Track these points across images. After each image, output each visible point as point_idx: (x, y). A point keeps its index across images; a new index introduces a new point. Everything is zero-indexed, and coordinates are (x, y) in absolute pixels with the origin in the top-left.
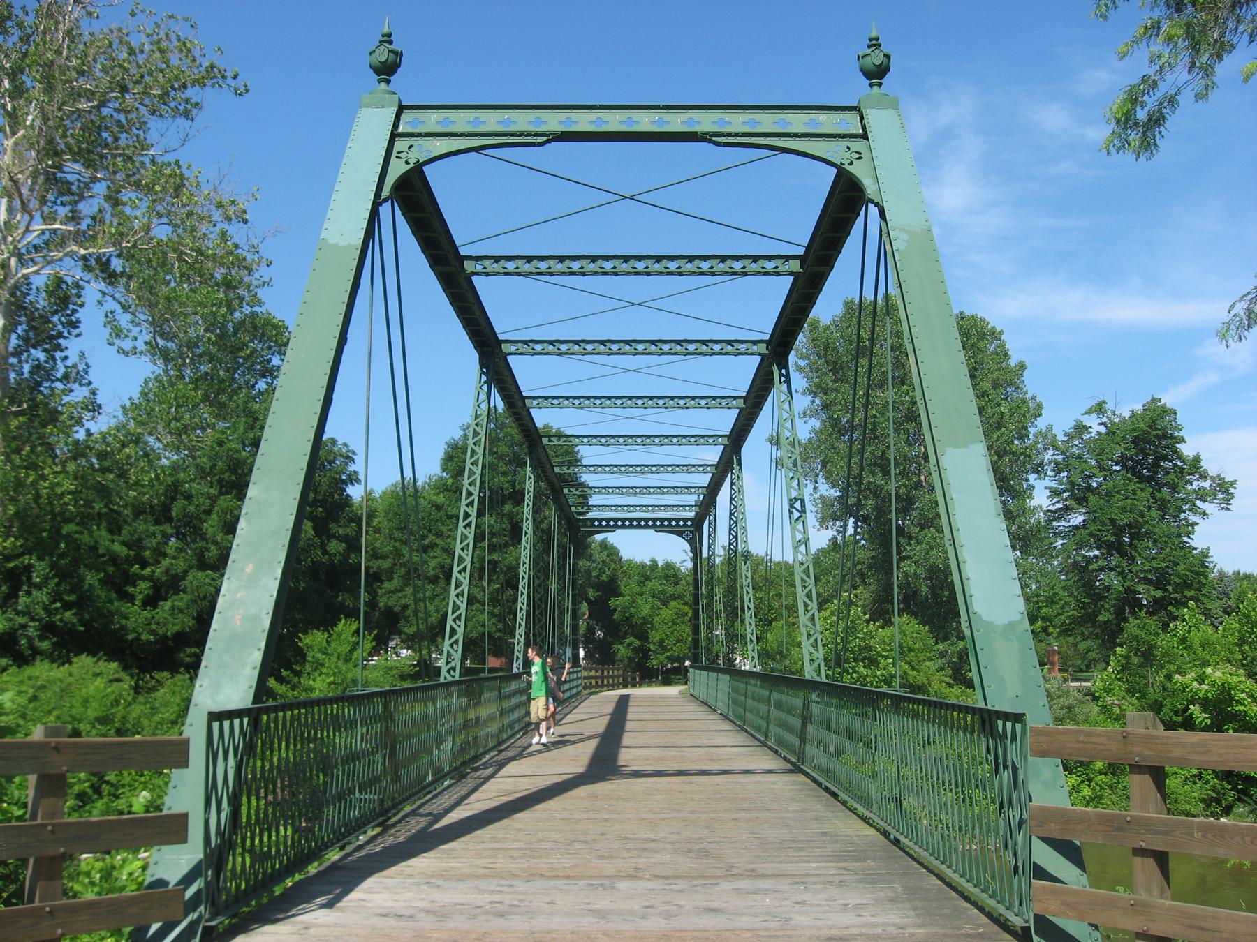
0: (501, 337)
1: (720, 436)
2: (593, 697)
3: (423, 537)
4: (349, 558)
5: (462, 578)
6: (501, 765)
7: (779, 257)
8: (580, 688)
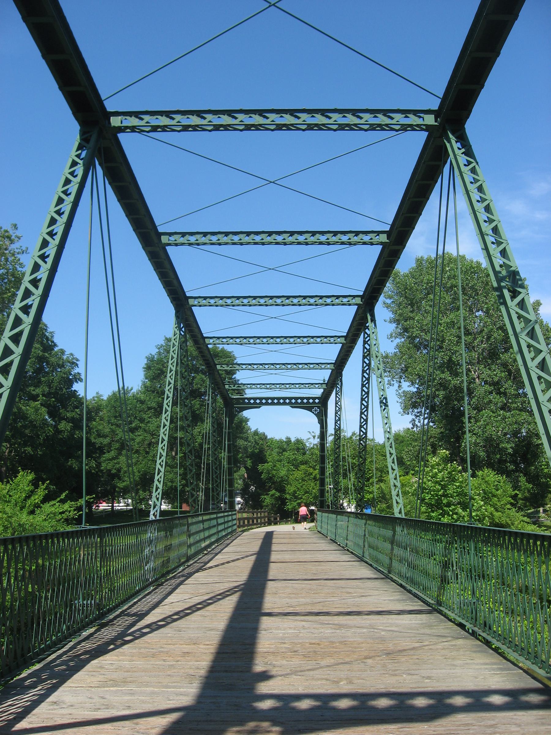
0: (188, 295)
1: (328, 364)
2: (245, 533)
3: (131, 423)
4: (75, 434)
5: (162, 449)
6: (190, 575)
7: (373, 232)
8: (235, 527)
